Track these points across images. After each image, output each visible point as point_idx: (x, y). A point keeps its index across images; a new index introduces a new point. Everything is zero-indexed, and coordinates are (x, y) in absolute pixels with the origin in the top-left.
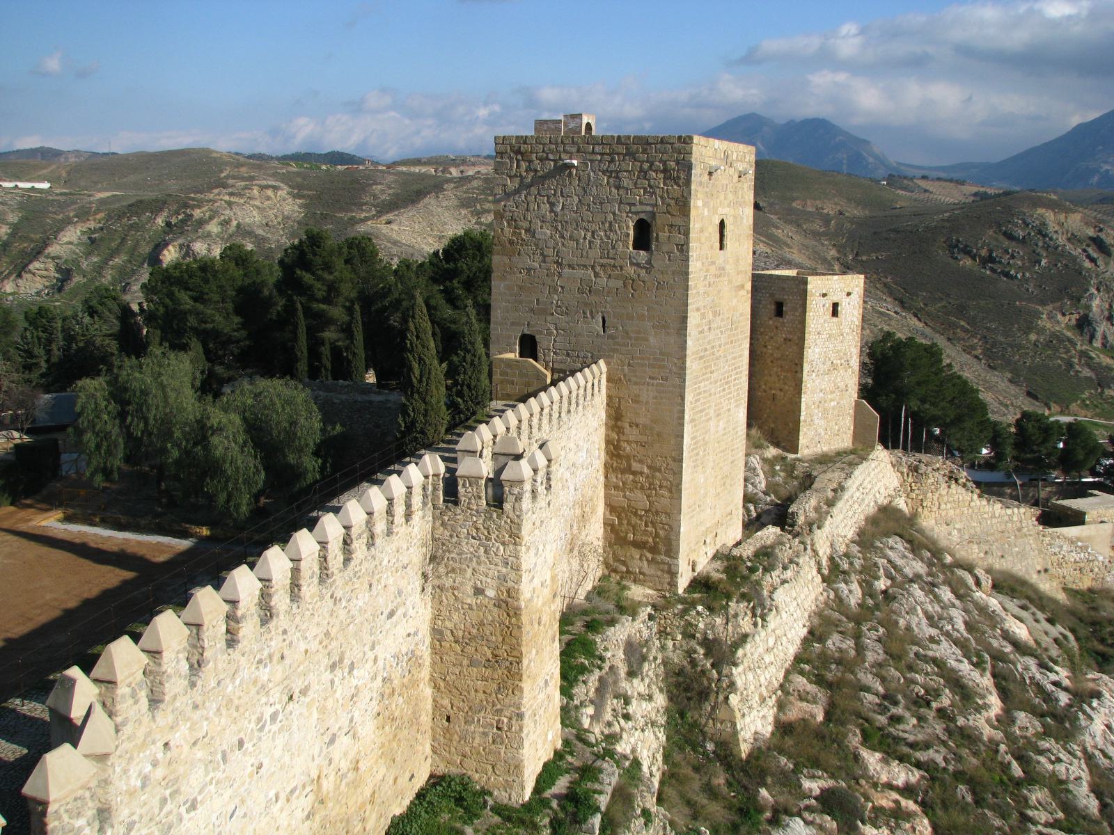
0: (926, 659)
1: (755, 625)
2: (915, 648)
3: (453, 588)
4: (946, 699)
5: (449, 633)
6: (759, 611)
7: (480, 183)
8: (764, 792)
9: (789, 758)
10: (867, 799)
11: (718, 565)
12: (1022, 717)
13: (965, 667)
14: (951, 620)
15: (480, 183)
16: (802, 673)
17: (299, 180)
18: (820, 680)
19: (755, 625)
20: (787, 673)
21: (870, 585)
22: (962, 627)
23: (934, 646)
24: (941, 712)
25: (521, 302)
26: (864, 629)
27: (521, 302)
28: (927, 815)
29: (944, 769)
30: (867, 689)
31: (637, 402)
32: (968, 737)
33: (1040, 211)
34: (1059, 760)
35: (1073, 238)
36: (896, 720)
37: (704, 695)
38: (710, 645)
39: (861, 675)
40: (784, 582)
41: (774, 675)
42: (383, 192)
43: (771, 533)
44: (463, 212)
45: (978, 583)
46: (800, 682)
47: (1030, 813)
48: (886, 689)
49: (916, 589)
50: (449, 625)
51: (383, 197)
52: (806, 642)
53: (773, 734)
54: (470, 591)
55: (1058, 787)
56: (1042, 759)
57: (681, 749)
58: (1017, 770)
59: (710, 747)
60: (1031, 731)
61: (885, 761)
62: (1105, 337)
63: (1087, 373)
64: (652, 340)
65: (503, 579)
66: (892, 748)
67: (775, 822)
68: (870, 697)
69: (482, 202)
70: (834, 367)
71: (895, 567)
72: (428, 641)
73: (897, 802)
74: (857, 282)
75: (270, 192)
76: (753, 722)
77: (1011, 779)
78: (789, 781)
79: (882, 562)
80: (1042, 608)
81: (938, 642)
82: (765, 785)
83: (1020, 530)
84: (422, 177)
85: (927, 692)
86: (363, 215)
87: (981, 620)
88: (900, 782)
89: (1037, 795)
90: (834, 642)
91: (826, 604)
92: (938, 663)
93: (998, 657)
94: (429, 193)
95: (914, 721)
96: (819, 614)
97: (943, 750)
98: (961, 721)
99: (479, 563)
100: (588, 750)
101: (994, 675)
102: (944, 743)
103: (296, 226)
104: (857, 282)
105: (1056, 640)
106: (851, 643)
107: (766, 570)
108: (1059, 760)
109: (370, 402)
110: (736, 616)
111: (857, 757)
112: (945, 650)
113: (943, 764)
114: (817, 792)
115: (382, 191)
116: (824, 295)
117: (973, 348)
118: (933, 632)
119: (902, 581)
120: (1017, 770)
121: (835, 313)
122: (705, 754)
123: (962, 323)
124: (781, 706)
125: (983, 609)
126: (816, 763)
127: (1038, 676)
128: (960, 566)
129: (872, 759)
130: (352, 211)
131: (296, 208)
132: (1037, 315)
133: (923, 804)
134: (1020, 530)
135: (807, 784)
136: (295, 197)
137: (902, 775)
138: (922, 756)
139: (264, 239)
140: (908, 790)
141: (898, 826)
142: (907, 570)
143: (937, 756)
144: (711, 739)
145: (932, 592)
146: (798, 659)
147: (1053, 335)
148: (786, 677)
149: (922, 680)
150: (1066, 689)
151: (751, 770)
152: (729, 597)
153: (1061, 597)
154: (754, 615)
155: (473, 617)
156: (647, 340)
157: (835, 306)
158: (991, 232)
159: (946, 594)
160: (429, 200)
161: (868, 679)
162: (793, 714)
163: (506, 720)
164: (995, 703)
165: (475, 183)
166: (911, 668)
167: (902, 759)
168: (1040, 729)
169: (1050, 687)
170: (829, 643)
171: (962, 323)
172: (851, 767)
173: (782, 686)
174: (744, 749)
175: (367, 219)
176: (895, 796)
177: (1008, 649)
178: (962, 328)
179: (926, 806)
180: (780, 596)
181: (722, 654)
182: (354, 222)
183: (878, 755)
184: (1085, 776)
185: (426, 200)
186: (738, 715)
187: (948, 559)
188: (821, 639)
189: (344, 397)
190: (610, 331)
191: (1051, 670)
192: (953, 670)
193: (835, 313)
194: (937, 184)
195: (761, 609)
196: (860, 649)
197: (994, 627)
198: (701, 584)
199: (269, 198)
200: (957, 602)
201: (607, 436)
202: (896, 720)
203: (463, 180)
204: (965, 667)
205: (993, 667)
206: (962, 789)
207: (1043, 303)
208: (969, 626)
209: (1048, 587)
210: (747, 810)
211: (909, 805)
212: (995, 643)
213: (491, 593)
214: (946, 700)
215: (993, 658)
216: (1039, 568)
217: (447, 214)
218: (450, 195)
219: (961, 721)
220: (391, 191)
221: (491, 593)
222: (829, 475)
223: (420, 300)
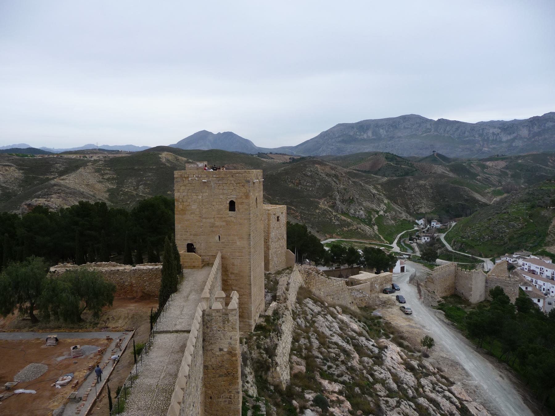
0: (332, 343)
1: (278, 340)
2: (328, 340)
3: (211, 350)
4: (342, 357)
5: (210, 366)
6: (279, 335)
7: (103, 162)
8: (294, 402)
9: (299, 387)
10: (328, 398)
11: (262, 319)
12: (366, 359)
13: (344, 344)
14: (334, 326)
15: (103, 162)
16: (295, 355)
17: (21, 162)
18: (301, 357)
19: (278, 340)
20: (290, 355)
21: (306, 318)
22: (338, 329)
23: (333, 338)
24: (343, 362)
25: (187, 232)
26: (310, 335)
27: (187, 232)
28: (348, 400)
29: (350, 382)
30: (318, 357)
31: (233, 265)
32: (352, 369)
33: (316, 166)
34: (382, 373)
35: (328, 175)
36: (330, 367)
37: (268, 369)
38: (267, 350)
39: (314, 352)
40: (283, 322)
41: (287, 358)
42: (60, 167)
43: (274, 304)
44: (97, 174)
45: (338, 312)
46: (294, 358)
47: (379, 393)
48: (324, 356)
49: (320, 318)
50: (210, 363)
51: (61, 169)
52: (293, 343)
53: (291, 379)
54: (218, 350)
55: (383, 382)
56: (376, 373)
57: (263, 390)
58: (371, 380)
59: (272, 388)
60: (370, 364)
61: (330, 383)
62: (342, 209)
63: (337, 223)
64: (238, 243)
65: (230, 344)
66: (331, 378)
67: (302, 412)
68: (319, 360)
69: (104, 170)
70: (279, 239)
71: (311, 310)
72: (201, 370)
73: (337, 397)
74: (283, 208)
75: (7, 168)
76: (283, 375)
77: (370, 382)
78: (301, 396)
79: (307, 309)
80: (355, 317)
81: (333, 336)
82: (294, 399)
83: (342, 289)
84: (76, 160)
85: (336, 355)
86: (52, 177)
87: (343, 326)
88: (337, 390)
89: (378, 386)
90: (302, 341)
91: (295, 327)
92: (336, 344)
93: (353, 338)
94: (81, 167)
95: (335, 366)
96: (294, 331)
97: (347, 376)
98: (349, 364)
99: (221, 339)
100: (252, 399)
101: (353, 346)
102: (347, 373)
103: (21, 182)
104: (283, 208)
105: (363, 328)
106: (307, 341)
107: (278, 319)
108: (382, 373)
109: (118, 270)
110: (273, 337)
111: (320, 383)
112: (336, 339)
113: (348, 381)
114: (312, 399)
115: (60, 167)
116: (275, 214)
117: (297, 216)
118: (331, 332)
119: (315, 315)
120: (371, 380)
121: (278, 220)
122: (271, 390)
123: (293, 208)
124: (291, 368)
125: (342, 321)
126: (309, 388)
127: (366, 343)
128: (331, 306)
129: (325, 383)
130: (46, 175)
131: (20, 174)
132: (319, 203)
133: (346, 397)
134: (342, 289)
135: (308, 396)
136: (19, 169)
137: (337, 387)
138: (341, 379)
139: (7, 188)
140: (340, 393)
141: (340, 406)
142: (316, 311)
143: (346, 378)
144: (272, 385)
145: (325, 318)
146: (292, 350)
147: (325, 210)
148: (290, 357)
149: (334, 351)
150: (376, 347)
151: (289, 394)
152: (270, 332)
153: (358, 311)
154: (278, 336)
155: (219, 359)
156: (236, 243)
157: (278, 217)
158: (299, 174)
159: (329, 317)
160: (81, 170)
161: (316, 353)
162: (296, 371)
163: (233, 395)
164: (356, 355)
165: (100, 162)
166: (329, 347)
167: (336, 381)
168: (373, 362)
169: (371, 347)
170: (300, 342)
171: (293, 208)
172: (319, 388)
173: (290, 361)
174: (284, 386)
175: (54, 178)
176: (336, 395)
177: (355, 335)
178: (293, 209)
179: (348, 398)
180: (283, 328)
181: (271, 352)
182: (48, 180)
183: (327, 381)
184: (391, 377)
185: (80, 170)
186: (280, 375)
187: (327, 305)
188: (298, 341)
189: (106, 269)
190: (222, 241)
191: (370, 341)
192: (341, 346)
193: (278, 220)
194: (276, 155)
195: (279, 333)
196: (310, 342)
197: (348, 327)
198: (259, 327)
199: (7, 170)
200: (334, 320)
201: (222, 278)
202: (330, 367)
203: (95, 161)
204: (344, 344)
205: (352, 342)
206: (357, 389)
207: (320, 198)
208: (341, 328)
209: (354, 308)
210: (291, 410)
211: (341, 398)
212: (350, 333)
213: (225, 350)
214: (342, 357)
215: (352, 339)
216: (350, 302)
217: (89, 175)
218: (90, 168)
219: (349, 364)
220: (64, 167)
221: (225, 350)
222: (283, 279)
223: (426, 321)
